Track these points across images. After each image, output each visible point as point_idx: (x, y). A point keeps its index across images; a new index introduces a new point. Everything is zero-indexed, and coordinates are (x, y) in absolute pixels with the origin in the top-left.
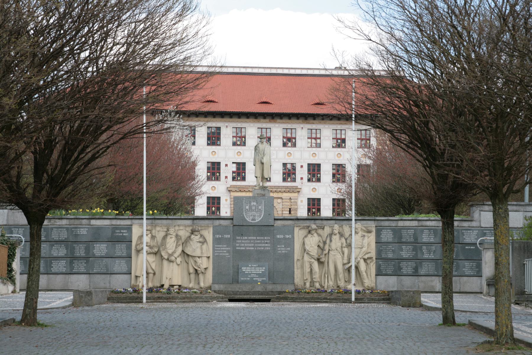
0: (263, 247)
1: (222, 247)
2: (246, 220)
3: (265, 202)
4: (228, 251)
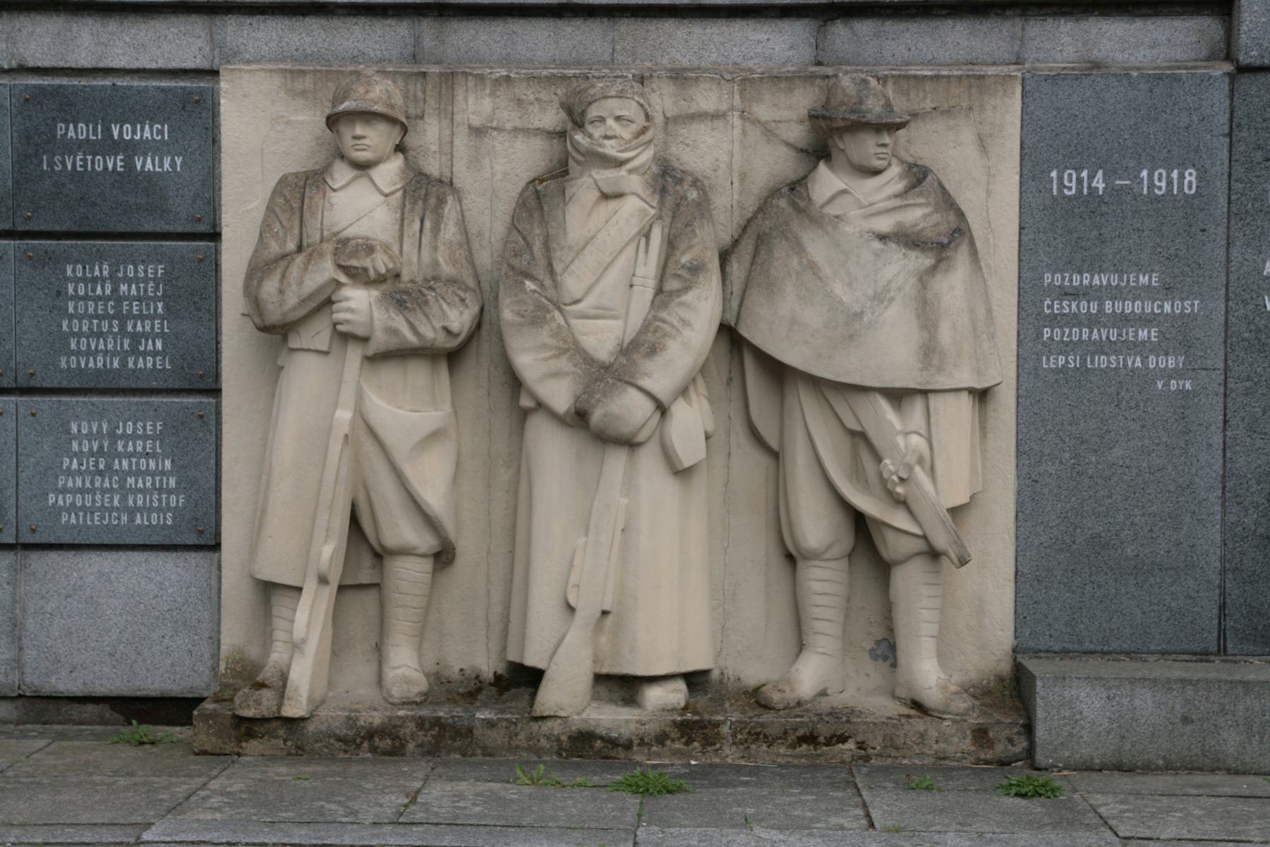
1: (1116, 294)
4: (1179, 335)
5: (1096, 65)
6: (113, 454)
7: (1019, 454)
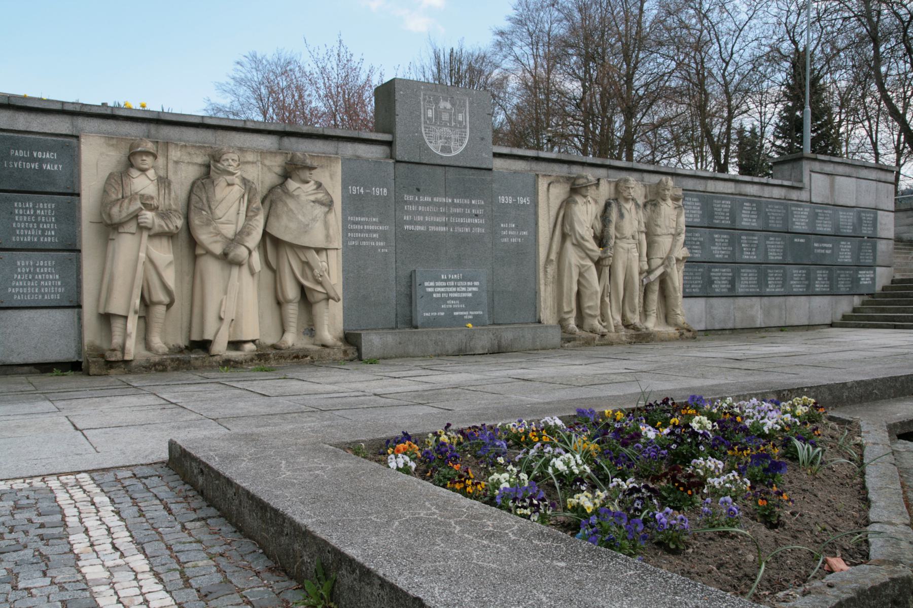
0: (469, 225)
1: (367, 223)
2: (428, 148)
3: (471, 103)
4: (384, 236)
5: (358, 157)
6: (35, 273)
7: (343, 271)
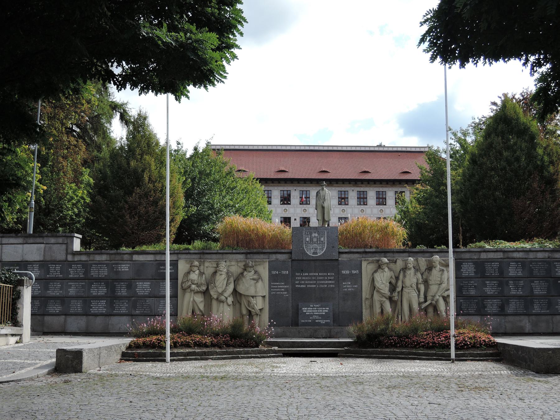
0: (326, 284)
1: (280, 285)
2: (307, 254)
3: (328, 233)
4: (286, 290)
